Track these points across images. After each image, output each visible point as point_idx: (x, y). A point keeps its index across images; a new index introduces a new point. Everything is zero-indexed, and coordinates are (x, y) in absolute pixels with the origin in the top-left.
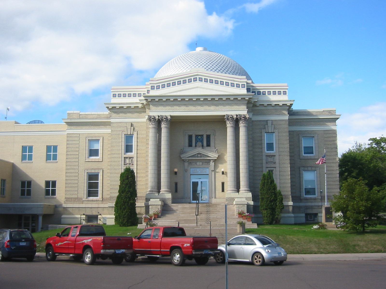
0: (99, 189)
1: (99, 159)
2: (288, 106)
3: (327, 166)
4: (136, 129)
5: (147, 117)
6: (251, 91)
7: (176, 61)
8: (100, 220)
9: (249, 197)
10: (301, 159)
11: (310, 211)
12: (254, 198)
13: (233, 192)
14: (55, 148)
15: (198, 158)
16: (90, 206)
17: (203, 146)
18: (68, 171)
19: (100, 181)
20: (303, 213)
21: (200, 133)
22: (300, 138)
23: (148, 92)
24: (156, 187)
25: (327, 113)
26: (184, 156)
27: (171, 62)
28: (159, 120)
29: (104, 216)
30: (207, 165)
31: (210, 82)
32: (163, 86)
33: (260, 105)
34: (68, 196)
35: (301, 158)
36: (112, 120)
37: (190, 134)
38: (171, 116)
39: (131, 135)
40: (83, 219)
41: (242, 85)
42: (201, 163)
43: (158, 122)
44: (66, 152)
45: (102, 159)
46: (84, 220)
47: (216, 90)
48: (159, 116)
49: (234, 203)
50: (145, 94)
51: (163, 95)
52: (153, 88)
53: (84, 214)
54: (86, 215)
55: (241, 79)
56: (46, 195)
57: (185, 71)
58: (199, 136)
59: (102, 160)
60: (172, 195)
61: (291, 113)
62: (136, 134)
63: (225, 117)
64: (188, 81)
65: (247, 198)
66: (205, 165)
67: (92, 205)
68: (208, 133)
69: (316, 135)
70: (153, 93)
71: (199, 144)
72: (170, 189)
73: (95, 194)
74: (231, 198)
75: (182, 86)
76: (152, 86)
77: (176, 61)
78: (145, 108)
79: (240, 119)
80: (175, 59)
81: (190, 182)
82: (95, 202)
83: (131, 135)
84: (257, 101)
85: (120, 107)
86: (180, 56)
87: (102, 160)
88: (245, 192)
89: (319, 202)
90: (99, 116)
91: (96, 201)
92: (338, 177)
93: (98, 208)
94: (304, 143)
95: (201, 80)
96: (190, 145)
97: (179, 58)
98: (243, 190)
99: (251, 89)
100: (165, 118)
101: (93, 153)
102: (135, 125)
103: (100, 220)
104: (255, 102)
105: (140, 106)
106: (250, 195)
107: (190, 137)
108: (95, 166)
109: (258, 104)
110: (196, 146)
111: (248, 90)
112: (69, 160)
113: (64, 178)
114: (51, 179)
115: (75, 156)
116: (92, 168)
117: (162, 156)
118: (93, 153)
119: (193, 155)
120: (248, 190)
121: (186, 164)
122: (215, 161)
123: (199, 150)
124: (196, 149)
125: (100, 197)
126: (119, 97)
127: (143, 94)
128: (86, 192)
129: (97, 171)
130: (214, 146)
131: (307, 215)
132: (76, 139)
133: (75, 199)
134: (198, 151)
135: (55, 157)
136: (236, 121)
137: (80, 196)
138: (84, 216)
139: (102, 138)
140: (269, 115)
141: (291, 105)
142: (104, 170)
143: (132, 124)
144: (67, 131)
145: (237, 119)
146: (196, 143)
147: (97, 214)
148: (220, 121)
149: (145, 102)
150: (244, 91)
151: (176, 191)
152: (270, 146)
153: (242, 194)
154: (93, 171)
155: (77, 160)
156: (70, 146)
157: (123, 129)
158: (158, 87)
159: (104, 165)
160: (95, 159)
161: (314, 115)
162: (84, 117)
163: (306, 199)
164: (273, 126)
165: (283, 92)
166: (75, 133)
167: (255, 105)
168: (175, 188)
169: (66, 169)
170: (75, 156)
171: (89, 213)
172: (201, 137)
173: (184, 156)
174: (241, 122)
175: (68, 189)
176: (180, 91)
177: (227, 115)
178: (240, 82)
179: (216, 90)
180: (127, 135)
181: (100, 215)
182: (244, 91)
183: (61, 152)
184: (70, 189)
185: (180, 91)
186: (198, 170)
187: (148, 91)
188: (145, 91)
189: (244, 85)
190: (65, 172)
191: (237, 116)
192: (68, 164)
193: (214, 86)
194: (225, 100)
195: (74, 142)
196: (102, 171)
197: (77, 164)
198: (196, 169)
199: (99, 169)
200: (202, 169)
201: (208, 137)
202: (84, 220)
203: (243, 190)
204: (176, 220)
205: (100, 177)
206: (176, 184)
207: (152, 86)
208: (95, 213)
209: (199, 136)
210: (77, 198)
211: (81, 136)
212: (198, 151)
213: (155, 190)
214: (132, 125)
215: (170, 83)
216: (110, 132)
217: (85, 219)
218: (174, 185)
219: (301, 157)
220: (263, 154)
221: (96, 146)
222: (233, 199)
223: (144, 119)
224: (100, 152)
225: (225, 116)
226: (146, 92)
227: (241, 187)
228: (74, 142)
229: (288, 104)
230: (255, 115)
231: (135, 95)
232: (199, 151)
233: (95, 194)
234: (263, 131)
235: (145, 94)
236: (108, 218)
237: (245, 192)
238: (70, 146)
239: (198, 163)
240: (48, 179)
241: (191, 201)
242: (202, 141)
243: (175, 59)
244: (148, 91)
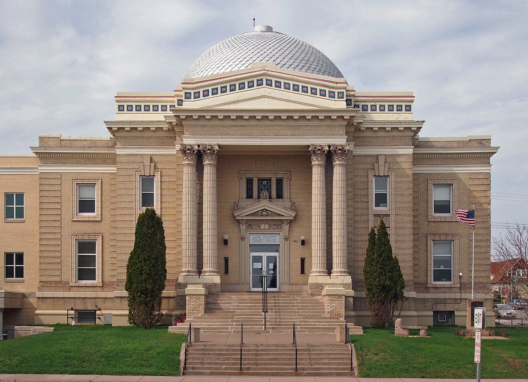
0: (96, 268)
1: (95, 217)
2: (413, 131)
3: (476, 234)
4: (159, 166)
5: (178, 147)
6: (353, 103)
7: (221, 49)
8: (99, 318)
9: (347, 284)
10: (429, 222)
11: (440, 308)
12: (355, 285)
13: (321, 274)
14: (20, 197)
15: (263, 218)
16: (82, 294)
17: (270, 197)
18: (43, 236)
19: (98, 254)
20: (430, 310)
21: (266, 176)
22: (429, 185)
23: (180, 102)
24: (195, 266)
25: (476, 144)
26: (241, 214)
27: (213, 49)
28: (199, 151)
29: (104, 312)
30: (277, 229)
31: (303, 91)
32: (206, 94)
33: (366, 128)
34: (44, 279)
35: (429, 220)
36: (118, 152)
37: (249, 176)
38: (219, 146)
39: (151, 177)
40: (70, 316)
41: (339, 93)
42: (267, 227)
43: (199, 156)
44: (40, 205)
45: (100, 216)
46: (72, 318)
47: (295, 102)
48: (199, 146)
49: (324, 292)
50: (174, 106)
51: (206, 108)
52: (188, 96)
53: (72, 309)
54: (76, 310)
55: (337, 83)
56: (6, 277)
57: (236, 68)
58: (265, 180)
59: (100, 220)
60: (221, 278)
61: (417, 144)
62: (160, 176)
63: (310, 149)
64: (248, 85)
65: (345, 285)
66: (274, 229)
67: (86, 292)
68: (280, 176)
69: (456, 182)
70: (188, 105)
71: (265, 193)
72: (218, 269)
73: (91, 275)
74: (318, 284)
75: (247, 93)
76: (186, 93)
77: (221, 49)
78: (174, 130)
79: (335, 151)
80: (219, 46)
81: (250, 257)
82: (91, 289)
83: (151, 177)
84: (362, 121)
85: (132, 129)
86: (227, 40)
87: (100, 220)
88: (340, 274)
89: (457, 293)
90: (94, 143)
91: (93, 287)
92: (167, 285)
93: (95, 298)
94: (440, 195)
95: (269, 84)
96: (249, 196)
97: (227, 44)
98: (337, 272)
99: (353, 100)
100: (209, 149)
101: (86, 206)
102: (155, 159)
103: (99, 318)
104: (358, 123)
105: (166, 127)
106: (348, 279)
107: (249, 182)
108: (88, 228)
109: (363, 127)
110: (259, 197)
111: (349, 102)
112: (45, 218)
113: (37, 248)
114: (14, 249)
115: (55, 212)
116: (85, 231)
117: (204, 213)
118: (86, 206)
119: (256, 212)
120: (345, 272)
121: (243, 227)
122: (290, 222)
123: (265, 204)
124: (259, 202)
125: (97, 281)
126: (147, 111)
127: (171, 106)
128: (75, 273)
129: (92, 238)
130: (289, 197)
131: (434, 312)
132: (55, 182)
133: (57, 282)
134: (262, 207)
135: (20, 213)
136: (329, 156)
137: (64, 278)
138: (72, 312)
139: (100, 181)
140: (381, 146)
141: (419, 129)
142: (104, 235)
143: (151, 159)
144: (39, 168)
145: (329, 152)
146: (259, 193)
147: (94, 308)
148: (302, 157)
149: (174, 121)
150: (342, 105)
151: (227, 272)
152: (381, 199)
153: (336, 277)
154: (86, 237)
155: (58, 218)
156: (46, 194)
157: (137, 166)
158: (197, 96)
159: (105, 228)
160: (89, 217)
161: (433, 147)
162: (67, 145)
163: (436, 288)
164: (387, 164)
165: (406, 106)
166: (52, 171)
167: (358, 129)
168: (225, 266)
169: (41, 233)
170: (55, 212)
171: (80, 306)
172: (267, 183)
173: (241, 214)
174: (336, 158)
175: (44, 267)
176: (234, 102)
177: (312, 145)
178: (336, 88)
179: (295, 102)
180: (145, 177)
181: (100, 309)
182: (342, 105)
183: (30, 204)
184: (48, 267)
185: (234, 102)
186: (262, 237)
187: (178, 100)
188: (174, 102)
189: (343, 93)
190: (38, 237)
191: (329, 146)
192: (43, 224)
193: (281, 93)
194: (335, 119)
195: (51, 188)
196: (101, 237)
197: (58, 224)
198: (259, 235)
199: (96, 234)
200: (268, 236)
201: (279, 182)
202: (72, 318)
203: (337, 272)
204: (171, 329)
205: (98, 248)
206: (226, 260)
207: (186, 93)
208: (90, 307)
209: (265, 180)
210: (60, 282)
211: (63, 178)
212: (262, 207)
213: (193, 270)
214: (151, 161)
215: (217, 89)
216: (116, 172)
217: (73, 316)
218: (223, 262)
219: (429, 217)
220: (370, 213)
221: (86, 194)
222: (321, 286)
223: (174, 150)
224: (97, 205)
225: (309, 146)
226: (176, 104)
227: (334, 266)
228: (51, 188)
229: (414, 127)
230: (357, 146)
231: (156, 108)
232: (264, 206)
233: (91, 275)
234: (370, 173)
235: (174, 106)
236: (117, 313)
237: (340, 274)
238: (46, 194)
239: (262, 227)
240: (10, 250)
241: (250, 288)
242: (269, 190)
243: (219, 46)
244: (178, 100)
